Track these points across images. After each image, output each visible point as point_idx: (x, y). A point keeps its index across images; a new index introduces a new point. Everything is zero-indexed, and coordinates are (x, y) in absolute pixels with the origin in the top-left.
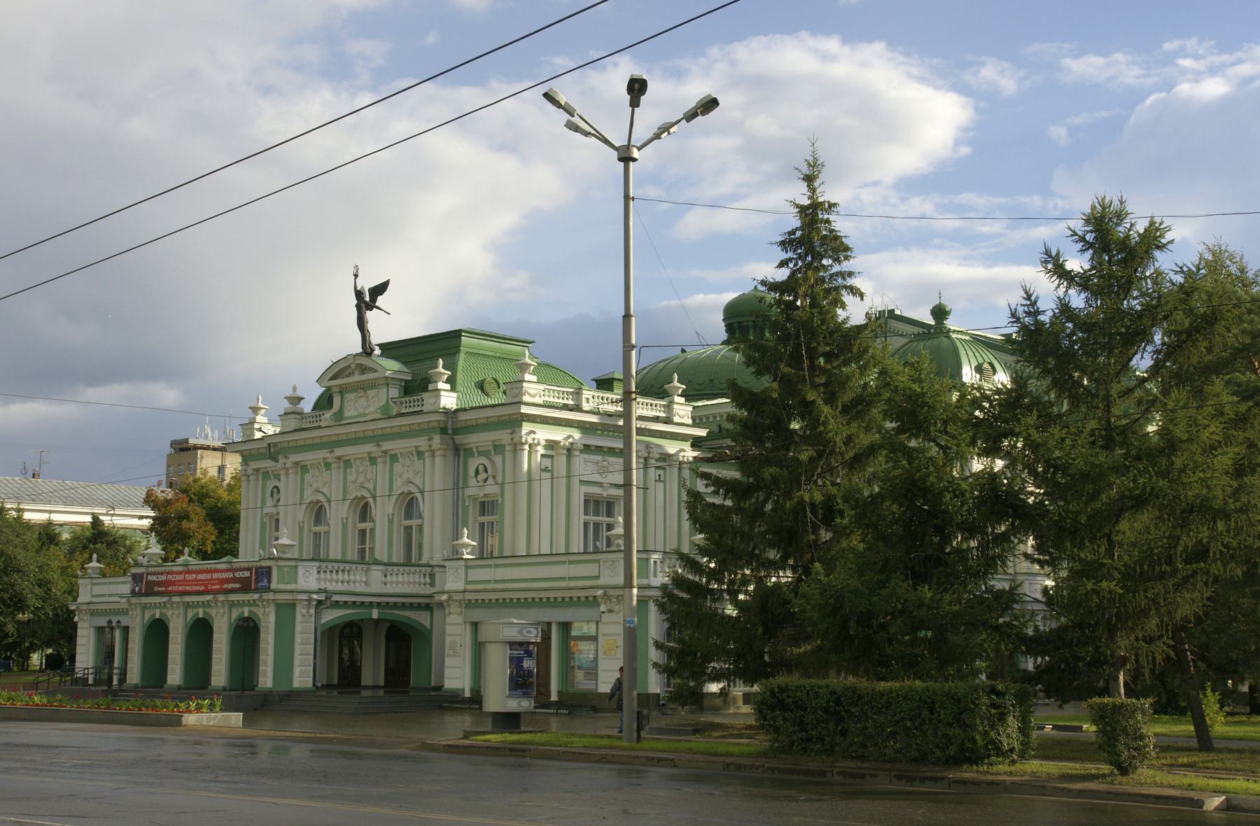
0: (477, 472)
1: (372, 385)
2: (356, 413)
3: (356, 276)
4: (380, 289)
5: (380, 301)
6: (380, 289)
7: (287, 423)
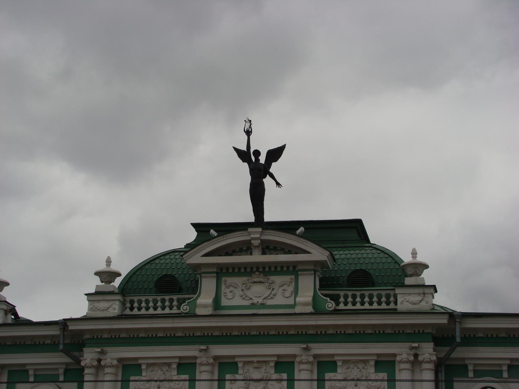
1: (292, 270)
2: (247, 303)
3: (248, 133)
4: (275, 154)
5: (274, 168)
6: (275, 154)
7: (103, 305)
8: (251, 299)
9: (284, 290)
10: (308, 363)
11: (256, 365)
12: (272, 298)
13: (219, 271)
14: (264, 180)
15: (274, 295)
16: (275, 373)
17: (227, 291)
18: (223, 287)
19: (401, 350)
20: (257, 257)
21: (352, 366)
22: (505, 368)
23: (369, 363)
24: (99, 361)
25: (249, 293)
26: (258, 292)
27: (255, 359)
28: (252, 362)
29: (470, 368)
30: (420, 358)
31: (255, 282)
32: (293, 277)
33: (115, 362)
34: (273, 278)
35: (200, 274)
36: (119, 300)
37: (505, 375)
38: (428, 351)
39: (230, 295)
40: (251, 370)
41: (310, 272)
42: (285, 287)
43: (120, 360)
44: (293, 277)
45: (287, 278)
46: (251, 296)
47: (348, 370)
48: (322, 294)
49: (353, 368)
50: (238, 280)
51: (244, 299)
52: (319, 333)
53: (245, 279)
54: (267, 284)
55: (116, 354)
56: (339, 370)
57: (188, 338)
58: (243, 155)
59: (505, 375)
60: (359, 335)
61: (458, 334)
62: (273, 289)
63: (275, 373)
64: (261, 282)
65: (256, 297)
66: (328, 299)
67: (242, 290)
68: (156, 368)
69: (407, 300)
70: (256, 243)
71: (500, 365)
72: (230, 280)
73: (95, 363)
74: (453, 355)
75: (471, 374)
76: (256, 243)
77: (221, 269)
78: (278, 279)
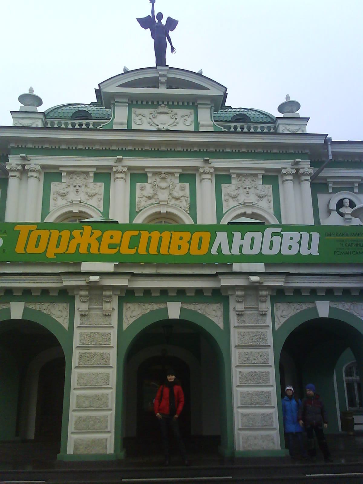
0: (340, 204)
8: (158, 125)
9: (185, 120)
10: (211, 173)
11: (163, 175)
12: (175, 125)
13: (130, 103)
14: (170, 31)
15: (177, 123)
16: (179, 183)
17: (137, 118)
18: (133, 115)
19: (285, 165)
20: (163, 90)
21: (243, 179)
22: (356, 185)
23: (258, 176)
24: (23, 166)
25: (155, 121)
26: (164, 120)
27: (163, 171)
28: (160, 173)
29: (331, 185)
30: (301, 171)
31: (160, 113)
32: (192, 110)
33: (38, 168)
34: (175, 111)
35: (114, 105)
36: (42, 118)
37: (356, 190)
38: (306, 166)
39: (139, 122)
40: (158, 180)
41: (207, 106)
42: (186, 118)
43: (43, 167)
44: (192, 110)
45: (187, 111)
46: (157, 124)
47: (240, 182)
48: (218, 125)
49: (244, 180)
50: (146, 112)
51: (151, 125)
52: (218, 151)
53: (152, 110)
54: (171, 115)
55: (37, 161)
56: (233, 181)
57: (105, 148)
58: (145, 22)
59: (356, 190)
60: (252, 152)
61: (330, 153)
62: (176, 119)
63: (179, 183)
64: (166, 113)
65: (162, 124)
66: (223, 128)
67: (150, 118)
68: (75, 177)
69: (288, 129)
70: (163, 80)
71: (353, 183)
72: (139, 111)
73: (20, 167)
74: (321, 174)
75: (330, 190)
76: (163, 80)
77: (132, 102)
78: (180, 112)
